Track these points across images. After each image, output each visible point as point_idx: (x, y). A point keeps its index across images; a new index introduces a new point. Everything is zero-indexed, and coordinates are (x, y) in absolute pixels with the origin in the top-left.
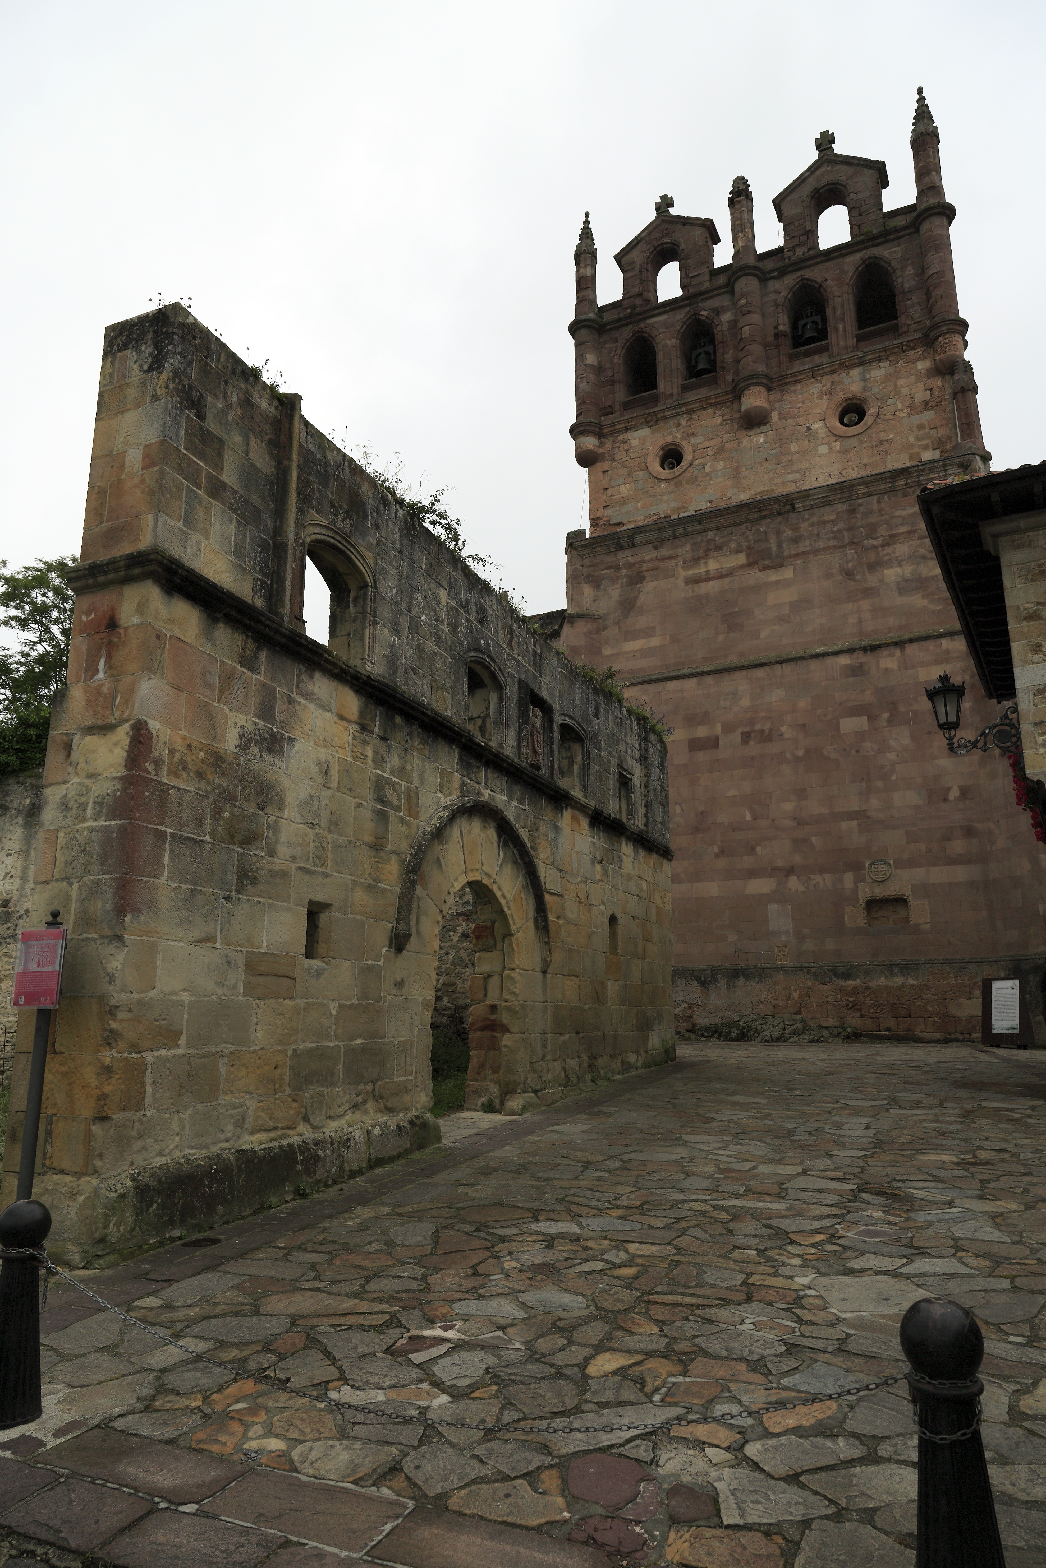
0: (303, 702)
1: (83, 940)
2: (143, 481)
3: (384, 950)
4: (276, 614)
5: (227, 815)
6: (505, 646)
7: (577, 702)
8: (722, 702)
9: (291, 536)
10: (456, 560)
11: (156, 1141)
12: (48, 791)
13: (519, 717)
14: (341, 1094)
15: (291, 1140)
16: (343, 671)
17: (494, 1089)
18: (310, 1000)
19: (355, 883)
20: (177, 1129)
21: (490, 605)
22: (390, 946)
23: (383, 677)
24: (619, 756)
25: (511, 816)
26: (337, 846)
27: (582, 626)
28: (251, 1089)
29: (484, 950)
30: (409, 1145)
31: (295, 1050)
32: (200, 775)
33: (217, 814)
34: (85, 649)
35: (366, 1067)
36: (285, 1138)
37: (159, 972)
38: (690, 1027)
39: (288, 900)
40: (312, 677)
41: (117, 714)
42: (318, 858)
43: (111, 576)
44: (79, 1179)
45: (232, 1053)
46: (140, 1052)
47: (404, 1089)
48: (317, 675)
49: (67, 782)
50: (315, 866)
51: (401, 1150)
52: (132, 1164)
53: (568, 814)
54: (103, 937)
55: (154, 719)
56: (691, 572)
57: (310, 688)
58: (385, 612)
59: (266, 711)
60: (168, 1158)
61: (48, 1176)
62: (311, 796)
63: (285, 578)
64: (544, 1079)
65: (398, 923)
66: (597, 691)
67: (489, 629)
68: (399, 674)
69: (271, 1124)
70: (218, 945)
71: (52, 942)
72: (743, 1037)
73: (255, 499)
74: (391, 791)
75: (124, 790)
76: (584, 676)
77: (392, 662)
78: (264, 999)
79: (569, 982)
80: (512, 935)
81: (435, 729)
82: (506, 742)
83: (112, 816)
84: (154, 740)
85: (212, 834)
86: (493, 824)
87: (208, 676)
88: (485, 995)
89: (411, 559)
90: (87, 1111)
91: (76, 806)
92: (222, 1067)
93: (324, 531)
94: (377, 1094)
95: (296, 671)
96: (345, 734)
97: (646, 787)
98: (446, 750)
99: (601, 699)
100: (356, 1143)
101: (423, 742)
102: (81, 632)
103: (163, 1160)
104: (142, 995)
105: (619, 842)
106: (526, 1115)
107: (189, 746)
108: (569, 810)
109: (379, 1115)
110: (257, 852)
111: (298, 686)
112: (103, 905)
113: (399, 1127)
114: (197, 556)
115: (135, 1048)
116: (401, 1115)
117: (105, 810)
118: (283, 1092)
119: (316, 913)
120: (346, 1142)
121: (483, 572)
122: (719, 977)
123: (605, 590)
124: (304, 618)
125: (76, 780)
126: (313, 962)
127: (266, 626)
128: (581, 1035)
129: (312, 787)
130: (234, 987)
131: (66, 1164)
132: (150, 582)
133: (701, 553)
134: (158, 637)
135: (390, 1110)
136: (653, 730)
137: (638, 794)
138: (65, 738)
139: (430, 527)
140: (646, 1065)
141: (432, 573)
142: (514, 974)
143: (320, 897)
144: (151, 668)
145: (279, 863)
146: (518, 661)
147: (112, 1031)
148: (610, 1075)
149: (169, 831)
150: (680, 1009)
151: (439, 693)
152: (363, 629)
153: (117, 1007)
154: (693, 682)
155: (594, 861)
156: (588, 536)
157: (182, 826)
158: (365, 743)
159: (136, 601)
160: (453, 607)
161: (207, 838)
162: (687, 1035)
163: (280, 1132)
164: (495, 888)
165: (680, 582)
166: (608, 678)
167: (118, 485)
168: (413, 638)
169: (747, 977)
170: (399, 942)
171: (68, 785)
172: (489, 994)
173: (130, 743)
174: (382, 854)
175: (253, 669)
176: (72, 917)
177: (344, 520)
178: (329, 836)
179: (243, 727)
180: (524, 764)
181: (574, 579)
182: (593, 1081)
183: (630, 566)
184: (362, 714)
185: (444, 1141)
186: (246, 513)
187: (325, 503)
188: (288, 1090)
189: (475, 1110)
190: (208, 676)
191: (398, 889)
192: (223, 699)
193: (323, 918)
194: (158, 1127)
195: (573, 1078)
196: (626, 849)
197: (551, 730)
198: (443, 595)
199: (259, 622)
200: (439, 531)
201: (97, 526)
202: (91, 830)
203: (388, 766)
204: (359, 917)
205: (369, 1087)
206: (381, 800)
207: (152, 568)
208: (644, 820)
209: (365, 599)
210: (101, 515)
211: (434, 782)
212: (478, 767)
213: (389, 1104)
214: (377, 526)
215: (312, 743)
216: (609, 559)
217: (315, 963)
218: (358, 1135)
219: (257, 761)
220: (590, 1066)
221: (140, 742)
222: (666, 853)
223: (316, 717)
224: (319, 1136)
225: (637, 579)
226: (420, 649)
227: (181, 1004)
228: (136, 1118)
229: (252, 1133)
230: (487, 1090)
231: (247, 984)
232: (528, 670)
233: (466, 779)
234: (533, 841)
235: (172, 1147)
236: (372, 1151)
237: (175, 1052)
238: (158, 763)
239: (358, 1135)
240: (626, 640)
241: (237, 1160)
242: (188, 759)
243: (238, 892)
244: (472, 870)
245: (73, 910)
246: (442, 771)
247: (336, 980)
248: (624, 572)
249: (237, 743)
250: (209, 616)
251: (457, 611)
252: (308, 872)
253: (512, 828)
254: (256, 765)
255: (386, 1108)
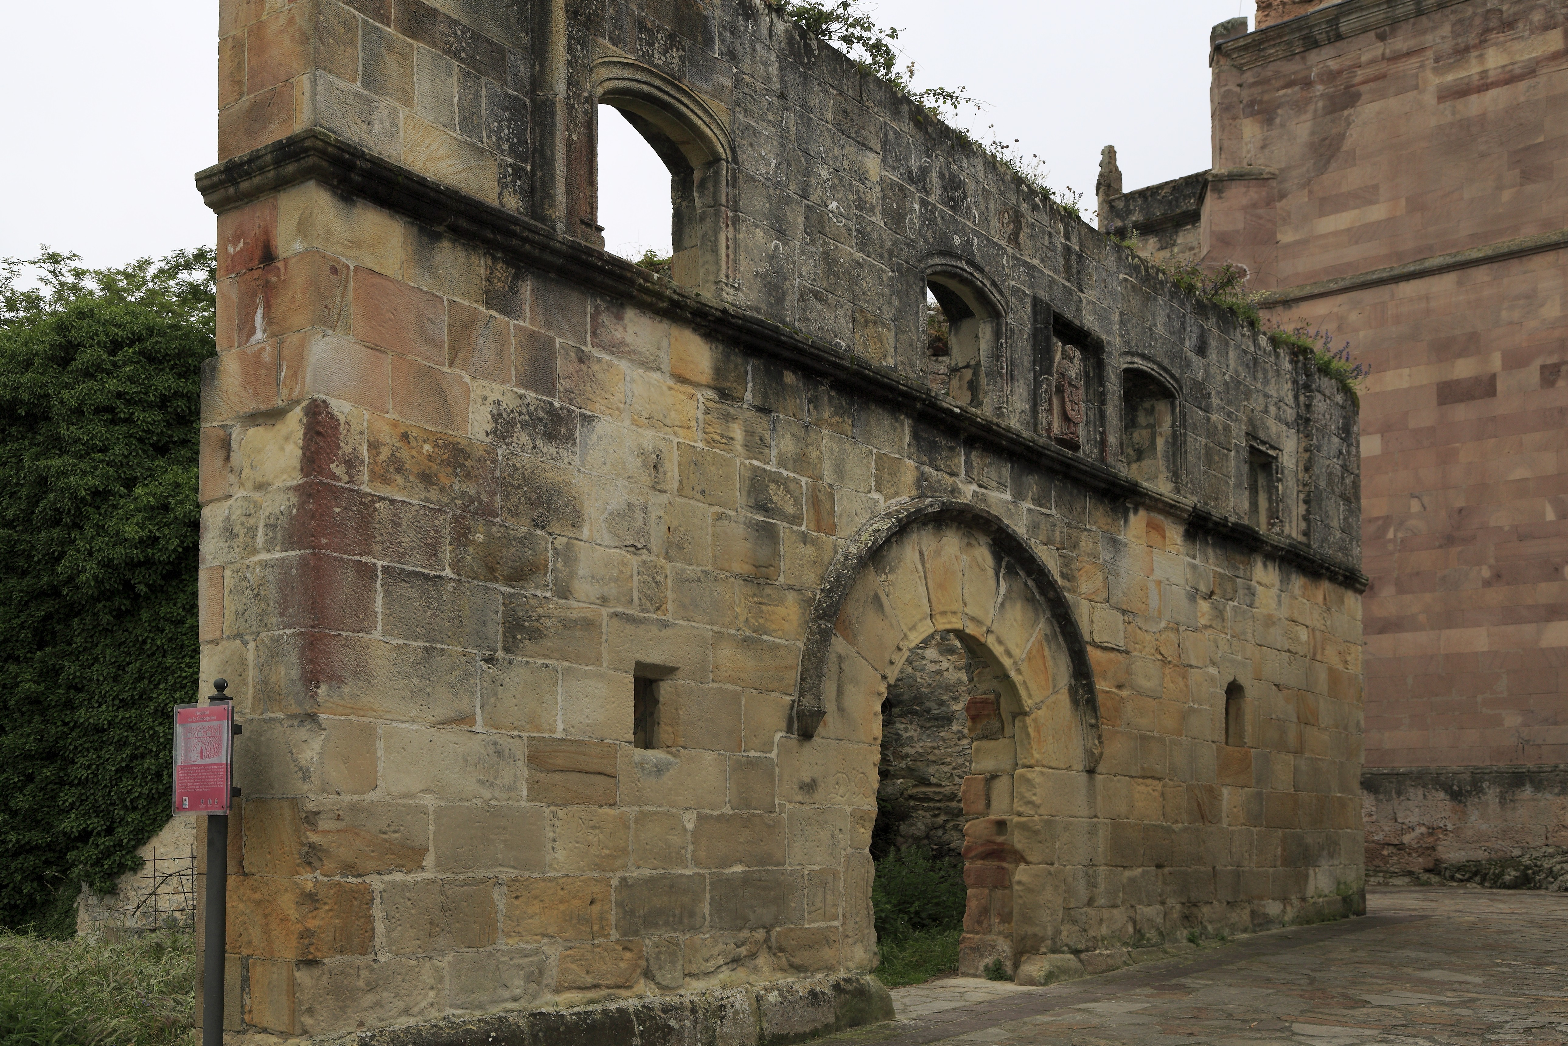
0: (607, 357)
1: (266, 721)
2: (291, 21)
3: (778, 736)
4: (543, 219)
5: (480, 537)
6: (1003, 243)
7: (1160, 329)
8: (1504, 314)
9: (560, 87)
10: (897, 99)
11: (397, 995)
12: (206, 512)
13: (1034, 363)
14: (709, 942)
15: (623, 1004)
16: (675, 304)
17: (1004, 947)
18: (647, 808)
19: (718, 636)
20: (430, 982)
21: (971, 174)
22: (789, 730)
23: (758, 310)
24: (1251, 421)
25: (1019, 527)
26: (682, 581)
27: (1239, 196)
28: (551, 930)
29: (985, 737)
30: (831, 1019)
31: (623, 879)
32: (427, 479)
33: (462, 536)
34: (235, 297)
35: (756, 907)
36: (613, 1000)
37: (381, 766)
38: (1431, 865)
39: (598, 661)
40: (619, 318)
41: (284, 392)
42: (649, 598)
43: (257, 180)
44: (286, 1040)
45: (514, 880)
46: (360, 875)
47: (824, 939)
48: (630, 314)
49: (230, 496)
50: (643, 611)
51: (818, 1025)
52: (361, 1024)
53: (1138, 521)
54: (291, 717)
55: (339, 397)
56: (1450, 78)
57: (618, 334)
58: (756, 202)
59: (539, 374)
60: (419, 1018)
61: (249, 1035)
62: (630, 505)
63: (554, 159)
64: (1092, 933)
65: (801, 694)
66: (1201, 309)
67: (968, 214)
68: (788, 304)
69: (589, 980)
70: (478, 728)
71: (215, 724)
72: (1526, 881)
73: (493, 31)
74: (781, 492)
75: (301, 506)
76: (1176, 285)
77: (774, 285)
78: (565, 805)
79: (1142, 788)
80: (1026, 714)
81: (862, 390)
82: (1011, 407)
83: (290, 543)
84: (342, 429)
85: (456, 566)
86: (984, 540)
87: (429, 326)
88: (988, 805)
89: (806, 107)
90: (289, 953)
91: (242, 532)
92: (500, 899)
93: (629, 73)
94: (774, 944)
95: (589, 309)
96: (692, 406)
97: (1307, 469)
98: (887, 422)
99: (1211, 324)
100: (736, 1013)
101: (839, 411)
102: (229, 271)
103: (412, 1022)
104: (356, 798)
105: (1249, 564)
106: (1052, 986)
107: (405, 436)
108: (1142, 513)
109: (779, 975)
110: (533, 590)
111: (594, 334)
112: (288, 671)
113: (813, 993)
114: (391, 134)
115: (348, 869)
116: (819, 976)
117: (279, 536)
118: (607, 936)
119: (656, 681)
120: (719, 1010)
121: (953, 118)
122: (1485, 785)
123: (1282, 125)
124: (600, 223)
125: (241, 493)
126: (649, 752)
127: (525, 240)
128: (1166, 870)
129: (631, 491)
130: (512, 788)
131: (268, 1020)
132: (312, 184)
133: (1472, 38)
134: (334, 270)
135: (799, 969)
136: (1325, 370)
137: (1291, 482)
138: (221, 433)
139: (842, 47)
140: (1303, 920)
141: (849, 126)
142: (1031, 774)
143: (655, 656)
144: (327, 319)
145: (577, 608)
146: (1031, 268)
147: (311, 846)
148: (1226, 932)
149: (379, 563)
150: (1413, 835)
151: (870, 330)
152: (716, 233)
153: (317, 813)
154: (1448, 280)
155: (1193, 596)
156: (1251, 28)
157: (402, 555)
158: (728, 418)
159: (296, 216)
160: (892, 184)
161: (448, 573)
162: (1425, 877)
163: (605, 992)
164: (991, 641)
165: (1429, 98)
166: (1223, 286)
167: (258, 30)
168: (813, 241)
169: (1538, 786)
170: (804, 725)
171: (231, 501)
172: (994, 804)
173: (305, 434)
174: (768, 590)
175: (508, 310)
176: (251, 690)
177: (665, 52)
178: (668, 566)
179: (498, 403)
180: (1042, 441)
181: (1225, 111)
182: (1191, 940)
183: (1331, 76)
184: (719, 372)
185: (898, 1017)
186: (476, 56)
187: (627, 24)
188: (614, 935)
189: (975, 976)
190: (429, 326)
191: (801, 645)
192: (457, 361)
193: (665, 689)
194: (400, 978)
195: (1151, 935)
196: (1264, 576)
197: (1101, 380)
198: (872, 164)
199: (512, 234)
200: (858, 53)
201: (236, 101)
202: (265, 565)
203: (774, 452)
204: (728, 687)
205: (760, 935)
206: (763, 507)
207: (311, 161)
208: (1303, 525)
209: (716, 183)
210: (240, 83)
211: (866, 477)
212: (952, 449)
213: (797, 961)
214: (732, 55)
215: (627, 423)
216: (1291, 68)
217: (653, 755)
218: (740, 1000)
219: (526, 452)
220: (1186, 917)
221: (319, 434)
222: (1350, 579)
223: (633, 381)
224: (671, 999)
225: (1346, 98)
226: (828, 259)
227: (423, 810)
228: (362, 964)
229: (557, 991)
230: (993, 947)
231: (533, 785)
232: (1053, 281)
233: (927, 469)
234: (1066, 565)
235: (424, 1004)
236: (765, 1025)
237: (419, 876)
238: (351, 464)
239: (740, 1000)
240: (1322, 214)
241: (532, 1026)
242: (404, 455)
243: (507, 650)
244: (944, 613)
245: (250, 679)
246: (880, 457)
247: (692, 780)
248: (1319, 88)
249: (489, 427)
250: (421, 230)
251: (901, 188)
252: (631, 619)
253: (1019, 545)
254: (526, 460)
255: (792, 966)
